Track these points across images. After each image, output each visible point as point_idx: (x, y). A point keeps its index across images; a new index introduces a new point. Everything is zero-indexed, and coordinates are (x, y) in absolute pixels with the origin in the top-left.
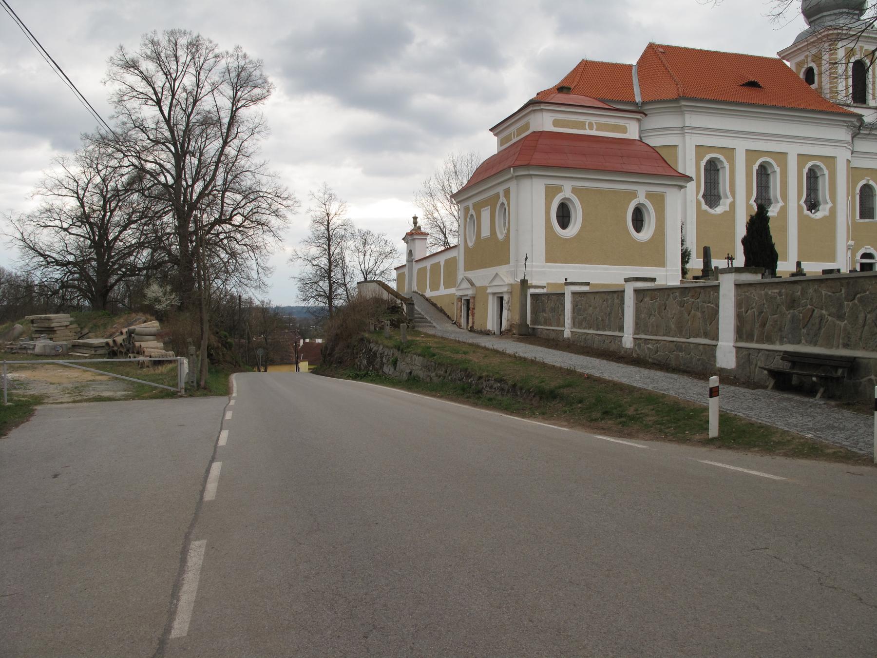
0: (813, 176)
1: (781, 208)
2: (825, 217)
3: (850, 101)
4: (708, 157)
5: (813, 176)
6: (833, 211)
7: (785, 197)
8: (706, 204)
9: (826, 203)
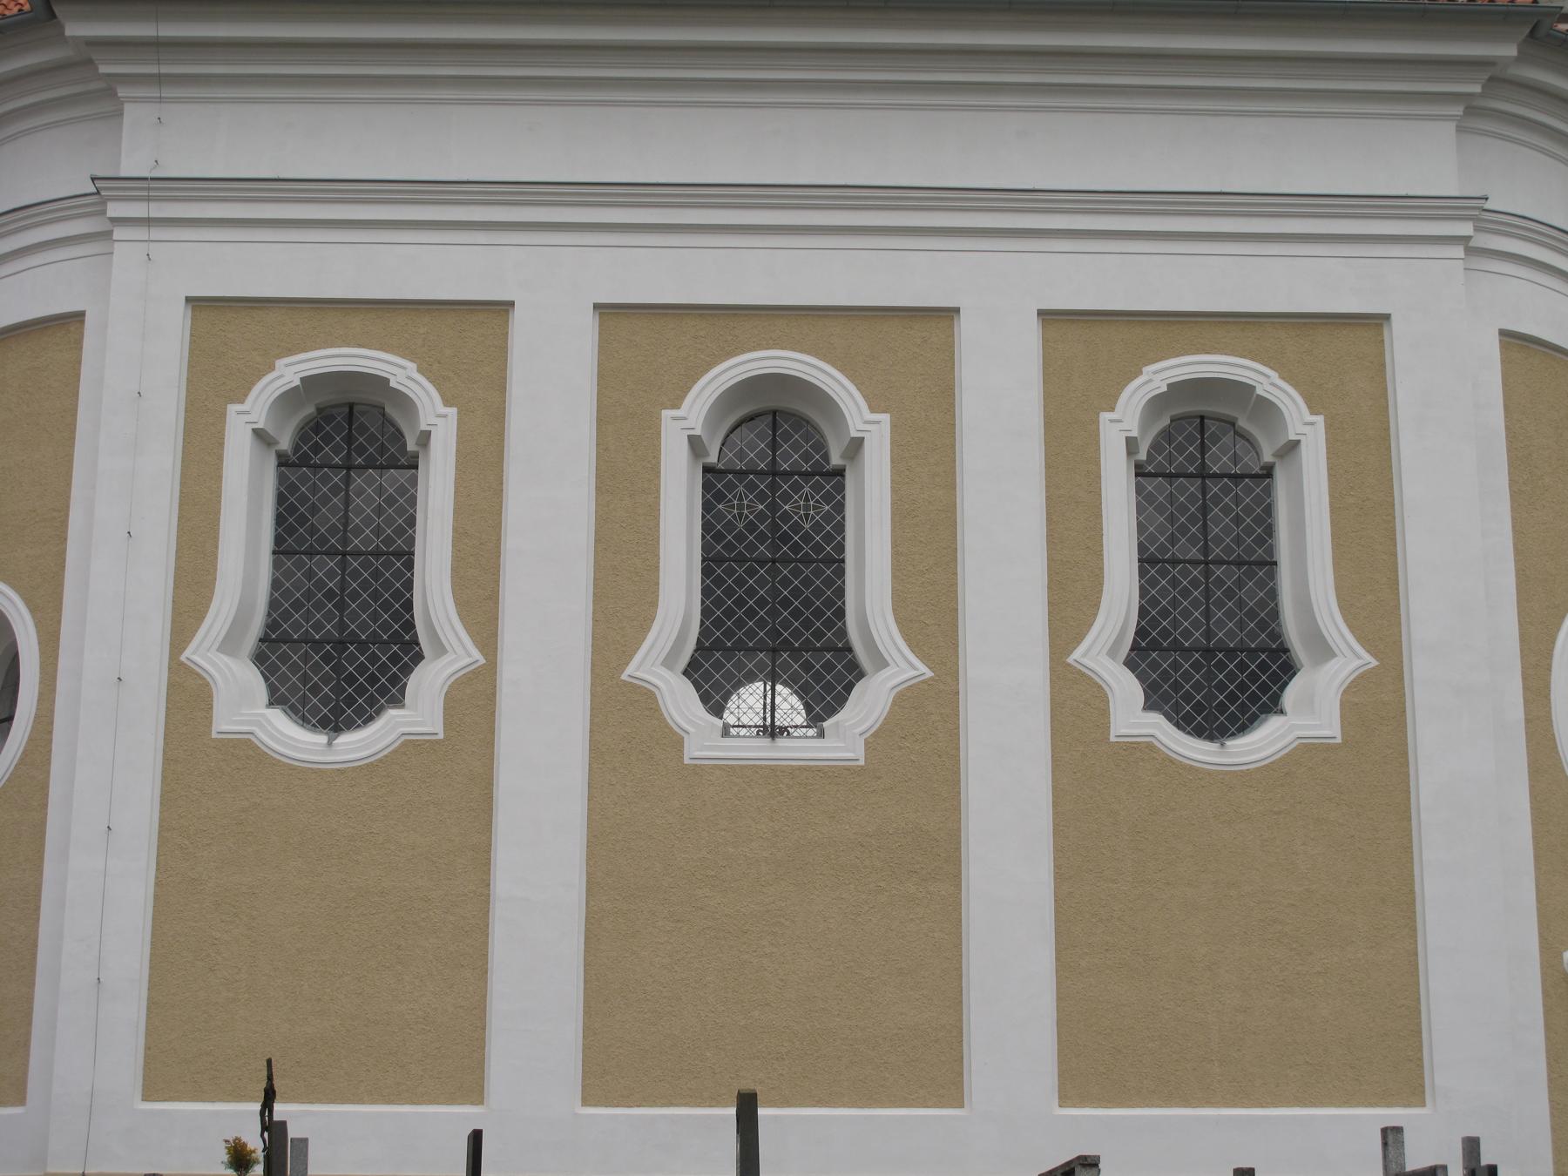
0: (1207, 482)
1: (907, 699)
2: (676, 742)
4: (1158, 376)
5: (1207, 482)
6: (1379, 708)
7: (932, 614)
8: (1155, 700)
9: (1324, 651)
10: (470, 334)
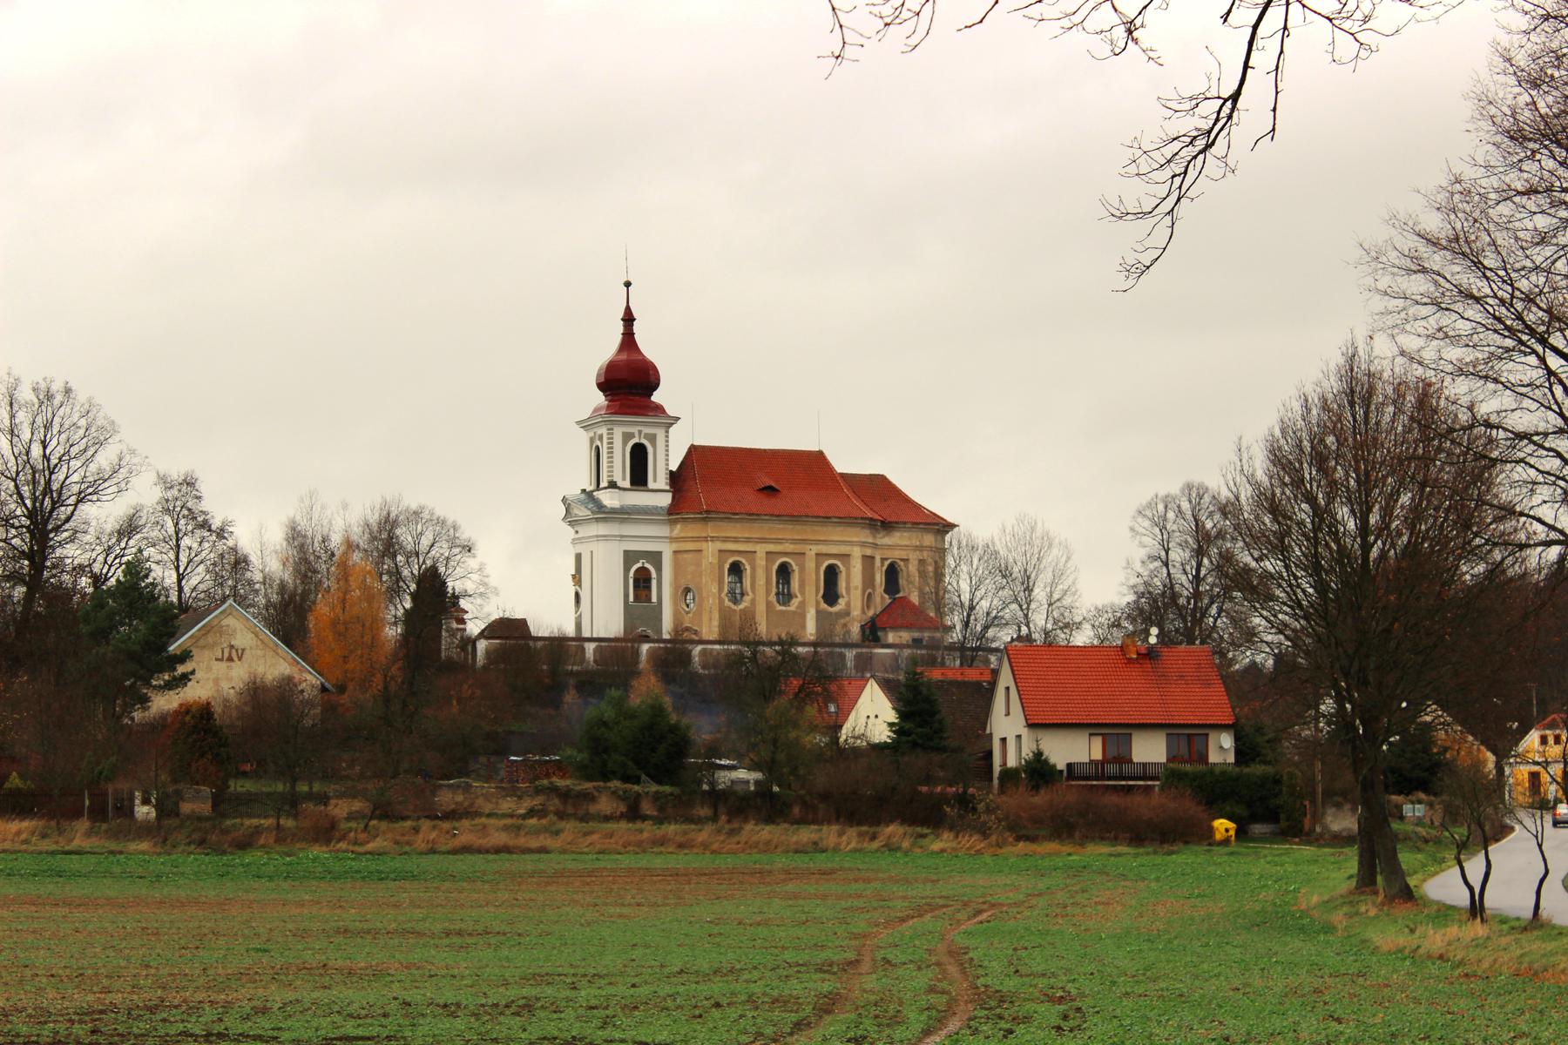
3: (627, 484)
4: (731, 560)
10: (845, 557)
